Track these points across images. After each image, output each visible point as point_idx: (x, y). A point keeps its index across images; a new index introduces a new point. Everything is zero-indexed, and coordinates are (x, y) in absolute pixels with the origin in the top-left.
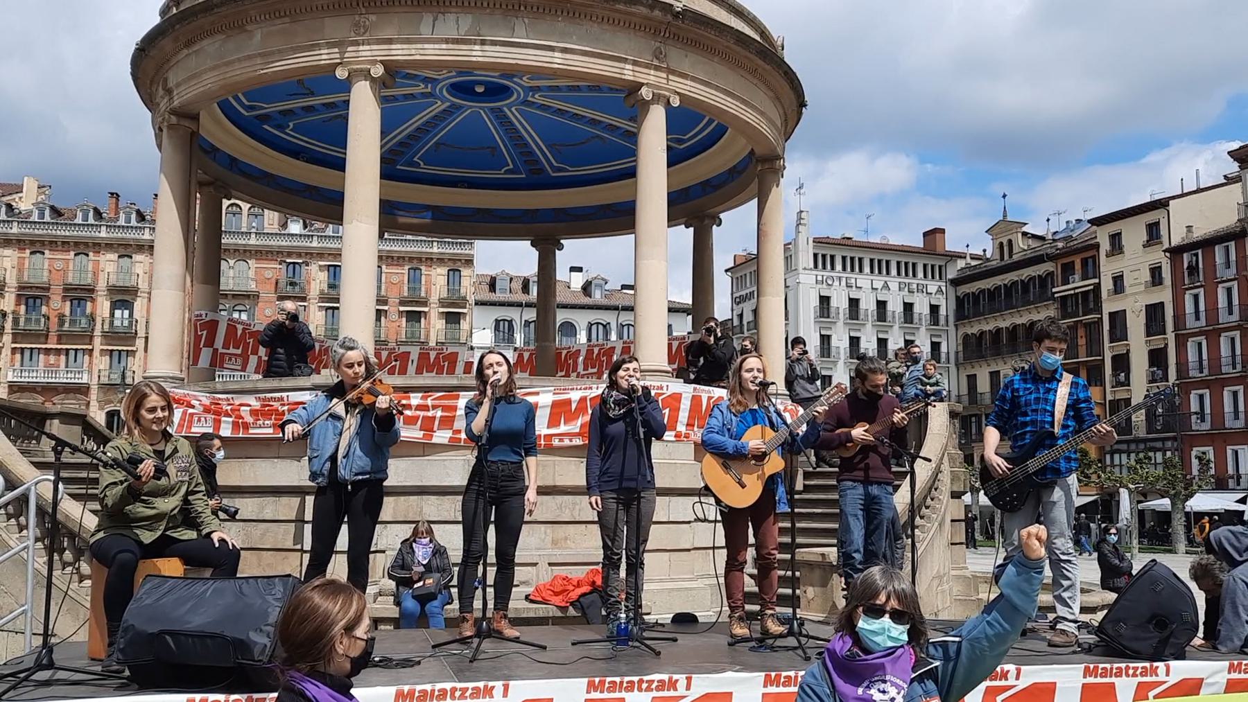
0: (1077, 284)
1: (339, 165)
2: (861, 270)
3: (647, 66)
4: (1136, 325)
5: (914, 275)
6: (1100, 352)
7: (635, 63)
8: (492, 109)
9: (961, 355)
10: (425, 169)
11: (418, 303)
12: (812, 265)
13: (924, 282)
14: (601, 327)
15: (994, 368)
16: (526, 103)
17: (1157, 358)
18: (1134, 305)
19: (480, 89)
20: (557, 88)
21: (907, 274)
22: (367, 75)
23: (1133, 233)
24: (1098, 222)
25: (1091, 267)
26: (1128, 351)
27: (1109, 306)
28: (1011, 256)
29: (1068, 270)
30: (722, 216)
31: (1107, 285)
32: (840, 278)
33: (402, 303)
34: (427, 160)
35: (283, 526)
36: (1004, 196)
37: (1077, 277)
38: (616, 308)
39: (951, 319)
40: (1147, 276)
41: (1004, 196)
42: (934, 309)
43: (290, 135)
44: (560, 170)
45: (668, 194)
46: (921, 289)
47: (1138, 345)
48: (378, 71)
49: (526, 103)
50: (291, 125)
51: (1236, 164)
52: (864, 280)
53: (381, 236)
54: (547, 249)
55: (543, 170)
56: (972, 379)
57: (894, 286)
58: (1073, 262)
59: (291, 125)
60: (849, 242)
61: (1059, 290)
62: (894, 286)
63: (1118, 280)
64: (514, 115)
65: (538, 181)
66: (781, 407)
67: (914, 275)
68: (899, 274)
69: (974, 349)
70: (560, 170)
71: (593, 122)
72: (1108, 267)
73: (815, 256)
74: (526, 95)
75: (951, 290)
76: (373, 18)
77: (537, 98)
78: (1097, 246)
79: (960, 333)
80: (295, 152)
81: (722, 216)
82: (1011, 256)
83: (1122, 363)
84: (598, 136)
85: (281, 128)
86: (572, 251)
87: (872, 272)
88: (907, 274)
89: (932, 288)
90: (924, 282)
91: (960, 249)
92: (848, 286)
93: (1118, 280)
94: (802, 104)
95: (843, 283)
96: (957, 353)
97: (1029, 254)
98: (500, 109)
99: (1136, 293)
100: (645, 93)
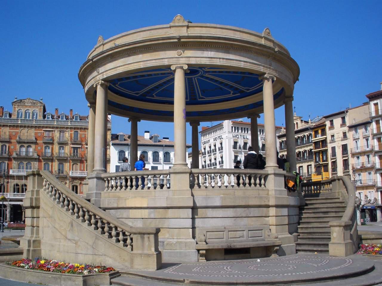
0: (320, 137)
1: (172, 103)
3: (267, 67)
7: (264, 66)
10: (156, 98)
12: (231, 131)
16: (202, 76)
17: (346, 163)
18: (338, 145)
20: (215, 72)
22: (182, 68)
23: (337, 121)
24: (326, 117)
25: (324, 133)
26: (336, 160)
28: (297, 128)
29: (316, 133)
31: (329, 139)
32: (241, 135)
33: (73, 144)
34: (157, 95)
36: (283, 124)
37: (320, 135)
38: (162, 146)
40: (341, 135)
41: (283, 124)
42: (245, 144)
45: (174, 105)
48: (186, 67)
49: (202, 76)
50: (119, 83)
59: (119, 83)
60: (241, 122)
61: (314, 139)
63: (333, 136)
66: (375, 204)
70: (203, 98)
71: (221, 83)
72: (329, 133)
73: (232, 127)
77: (207, 75)
78: (325, 125)
79: (69, 133)
82: (297, 128)
83: (334, 163)
86: (142, 124)
92: (244, 138)
93: (333, 136)
95: (242, 137)
97: (303, 127)
99: (339, 141)
100: (173, 68)
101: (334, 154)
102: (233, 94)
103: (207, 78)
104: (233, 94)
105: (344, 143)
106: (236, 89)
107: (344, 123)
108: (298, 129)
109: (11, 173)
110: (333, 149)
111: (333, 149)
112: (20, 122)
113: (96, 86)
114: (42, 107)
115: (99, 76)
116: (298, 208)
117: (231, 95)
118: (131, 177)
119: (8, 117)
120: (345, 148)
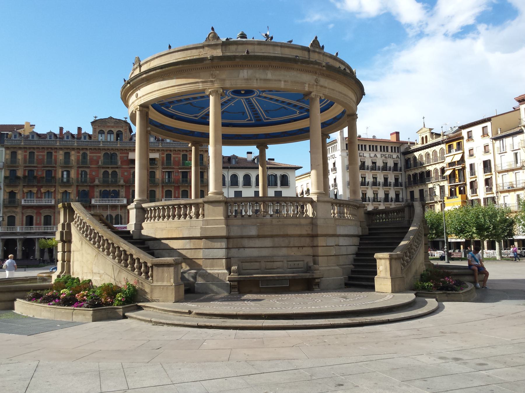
2: (365, 150)
4: (479, 169)
5: (387, 151)
6: (464, 180)
8: (246, 99)
9: (407, 183)
11: (186, 168)
12: (345, 148)
13: (391, 154)
14: (273, 177)
15: (421, 188)
16: (259, 96)
17: (488, 182)
19: (243, 92)
21: (384, 151)
25: (459, 147)
26: (476, 180)
27: (468, 161)
28: (426, 142)
30: (330, 135)
35: (325, 232)
36: (424, 118)
39: (403, 169)
41: (424, 118)
43: (171, 110)
44: (268, 119)
46: (391, 157)
47: (481, 177)
49: (259, 96)
51: (518, 103)
52: (366, 154)
53: (485, 173)
54: (262, 148)
55: (261, 120)
56: (412, 193)
57: (379, 155)
58: (452, 144)
62: (379, 155)
64: (254, 100)
65: (259, 123)
67: (387, 151)
68: (381, 151)
69: (56, 167)
70: (268, 119)
71: (283, 102)
72: (467, 146)
74: (260, 93)
75: (402, 157)
76: (218, 72)
77: (264, 95)
80: (171, 116)
81: (330, 135)
83: (473, 184)
84: (284, 107)
85: (167, 108)
87: (370, 150)
88: (384, 151)
89: (395, 156)
90: (391, 154)
91: (407, 140)
94: (363, 94)
96: (405, 182)
98: (248, 99)
101: (473, 173)
102: (300, 113)
103: (265, 97)
104: (300, 113)
105: (486, 157)
106: (301, 108)
107: (485, 134)
108: (427, 144)
109: (93, 202)
110: (472, 166)
111: (472, 166)
112: (101, 145)
113: (135, 112)
114: (128, 127)
115: (137, 101)
116: (359, 238)
117: (297, 115)
118: (163, 207)
119: (87, 139)
120: (487, 165)
